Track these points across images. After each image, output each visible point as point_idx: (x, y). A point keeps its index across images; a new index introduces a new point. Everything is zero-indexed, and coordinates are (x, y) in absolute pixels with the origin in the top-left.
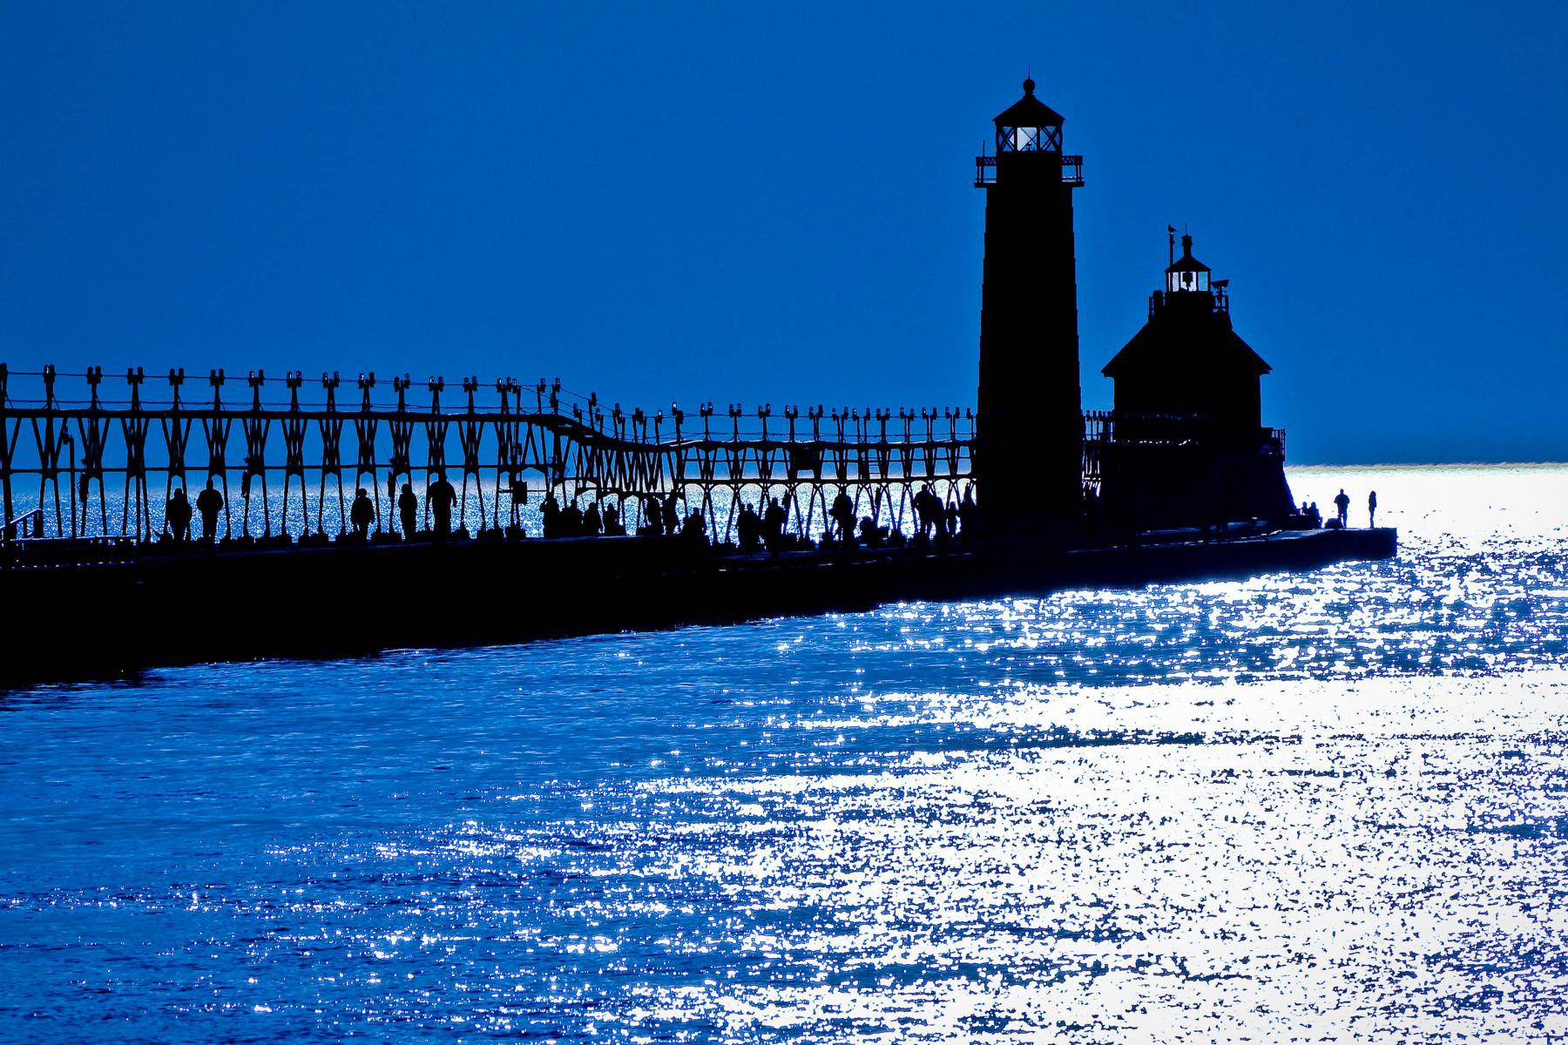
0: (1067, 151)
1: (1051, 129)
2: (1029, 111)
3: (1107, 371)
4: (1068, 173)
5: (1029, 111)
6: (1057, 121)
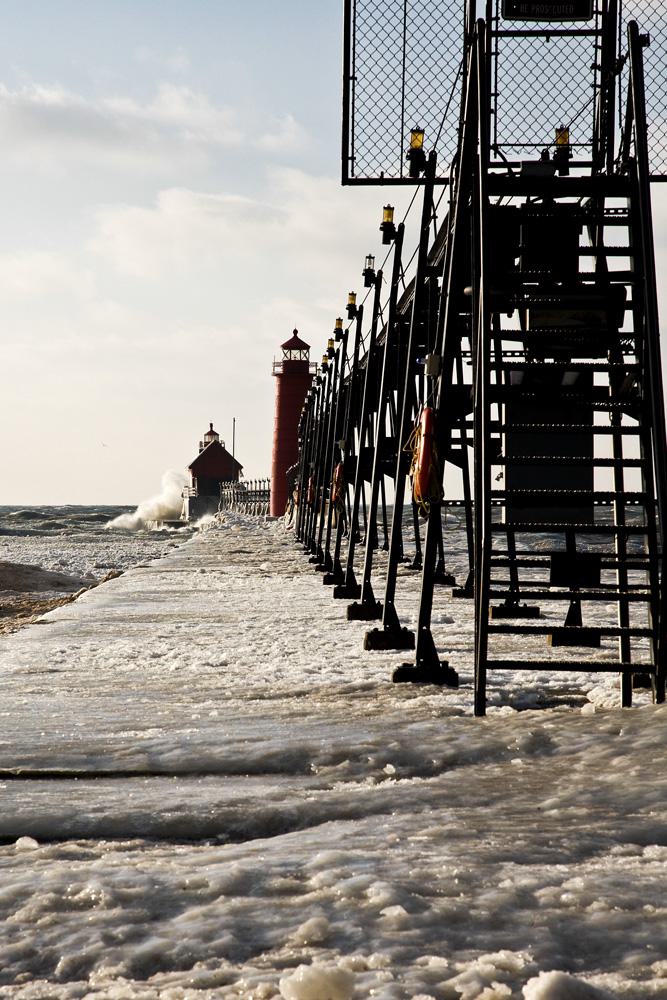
0: (311, 361)
1: (305, 351)
2: (295, 343)
3: (190, 468)
5: (295, 343)
6: (307, 347)
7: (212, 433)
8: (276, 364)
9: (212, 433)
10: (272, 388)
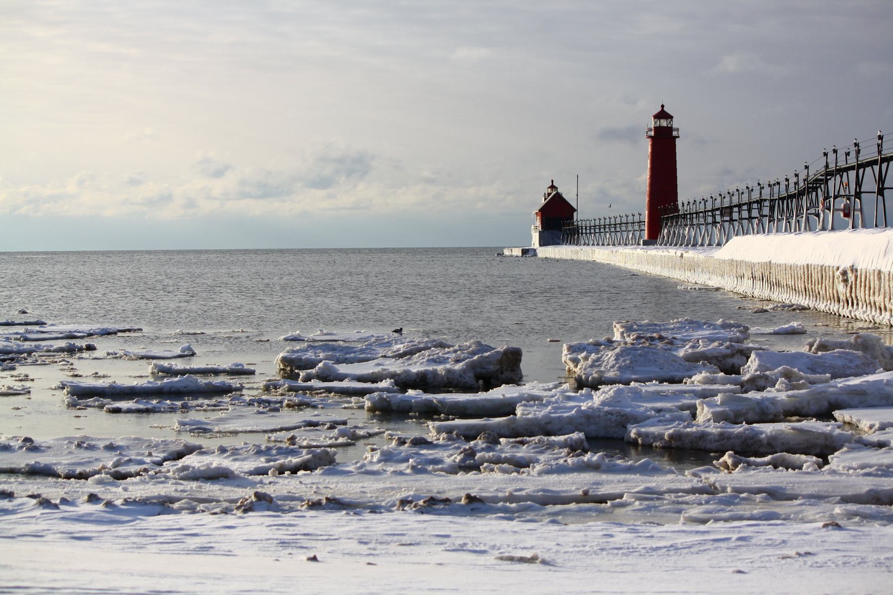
2: (662, 115)
4: (675, 133)
5: (662, 115)
6: (671, 117)
7: (553, 187)
8: (650, 130)
9: (553, 187)
10: (647, 147)
